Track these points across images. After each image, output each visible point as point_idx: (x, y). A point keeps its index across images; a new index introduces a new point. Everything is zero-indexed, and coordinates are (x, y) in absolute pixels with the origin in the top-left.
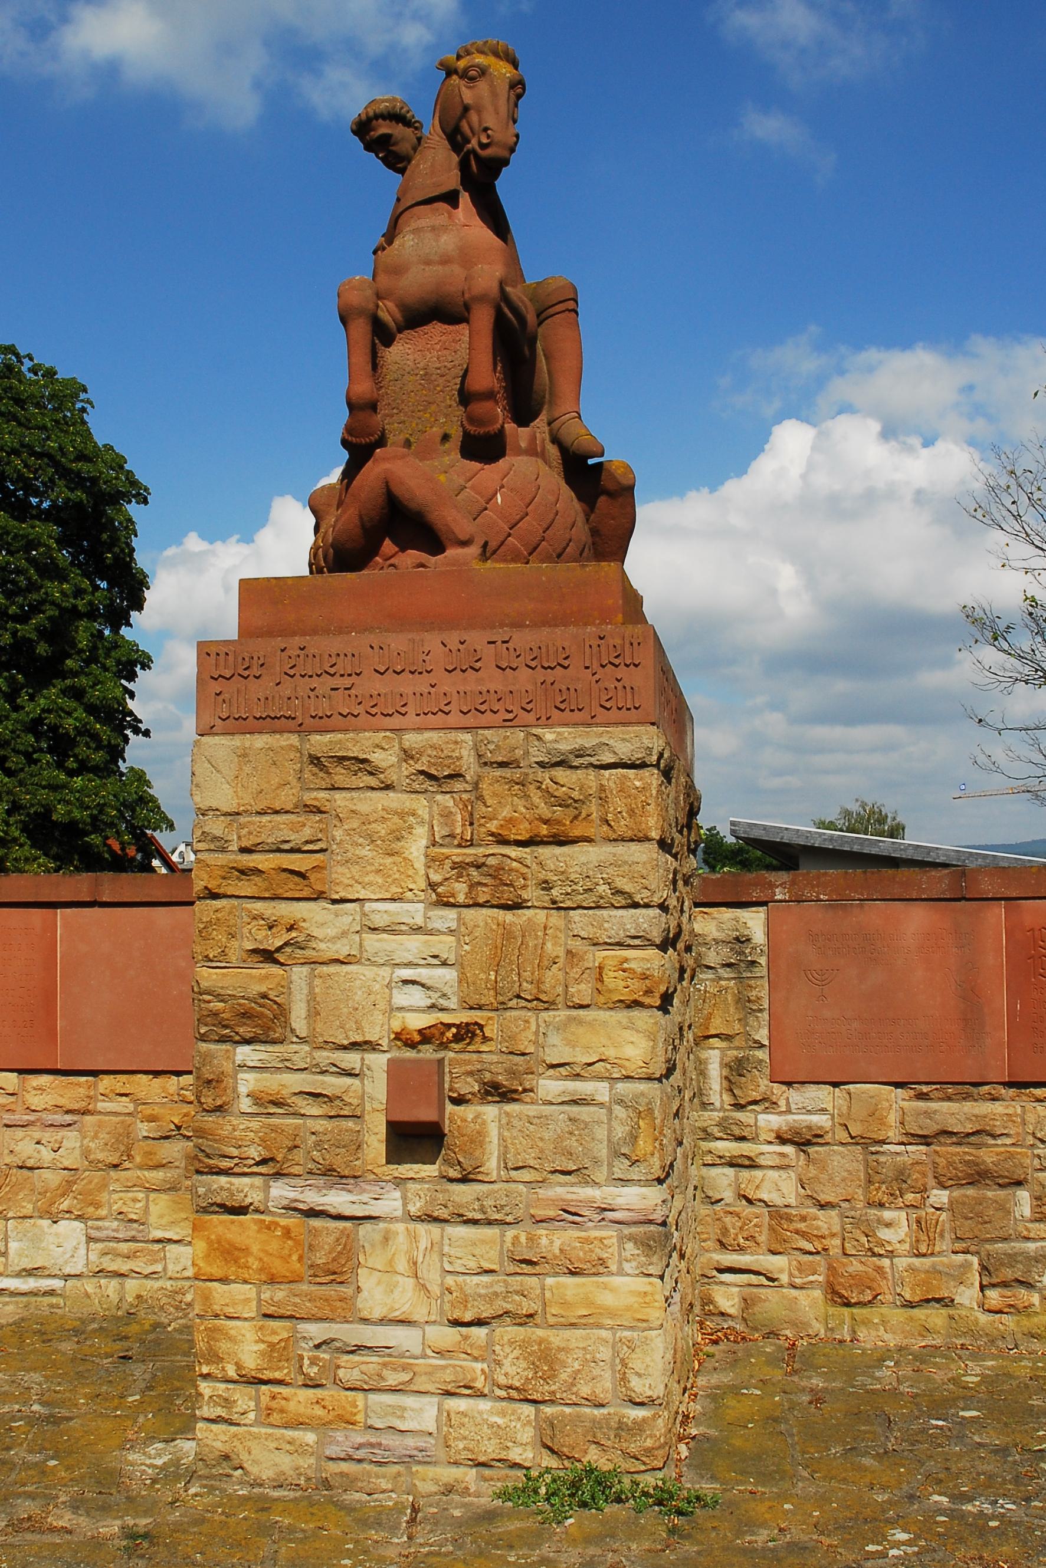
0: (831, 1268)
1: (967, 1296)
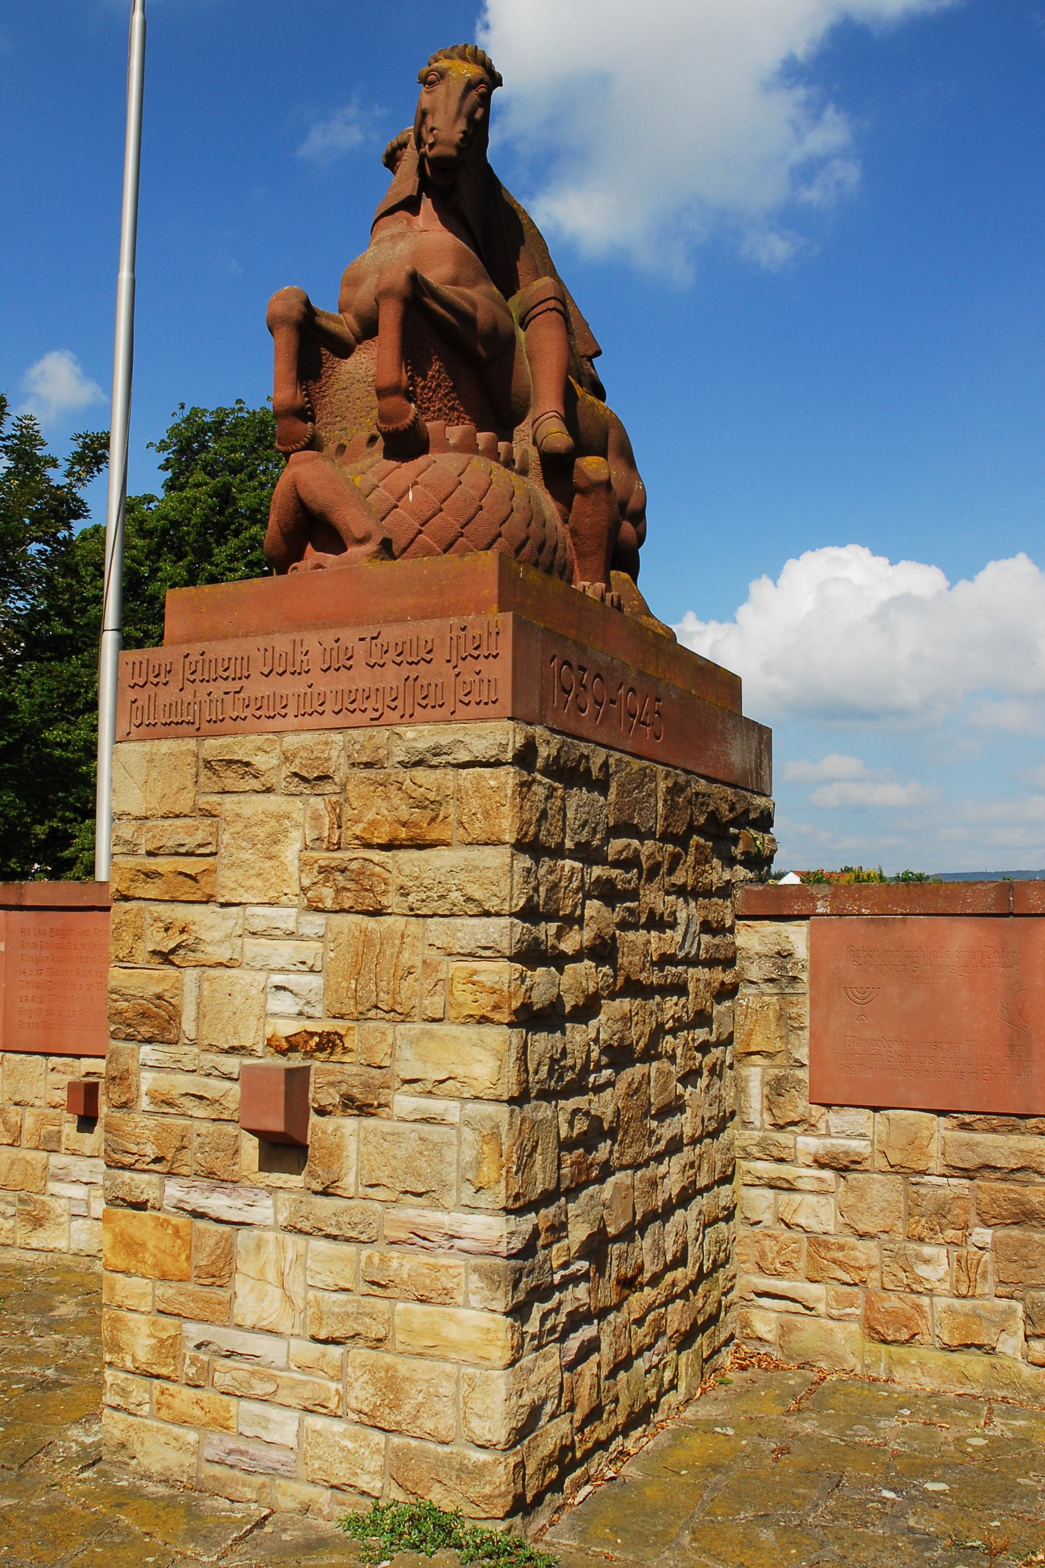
0: (868, 1301)
1: (1011, 1345)
